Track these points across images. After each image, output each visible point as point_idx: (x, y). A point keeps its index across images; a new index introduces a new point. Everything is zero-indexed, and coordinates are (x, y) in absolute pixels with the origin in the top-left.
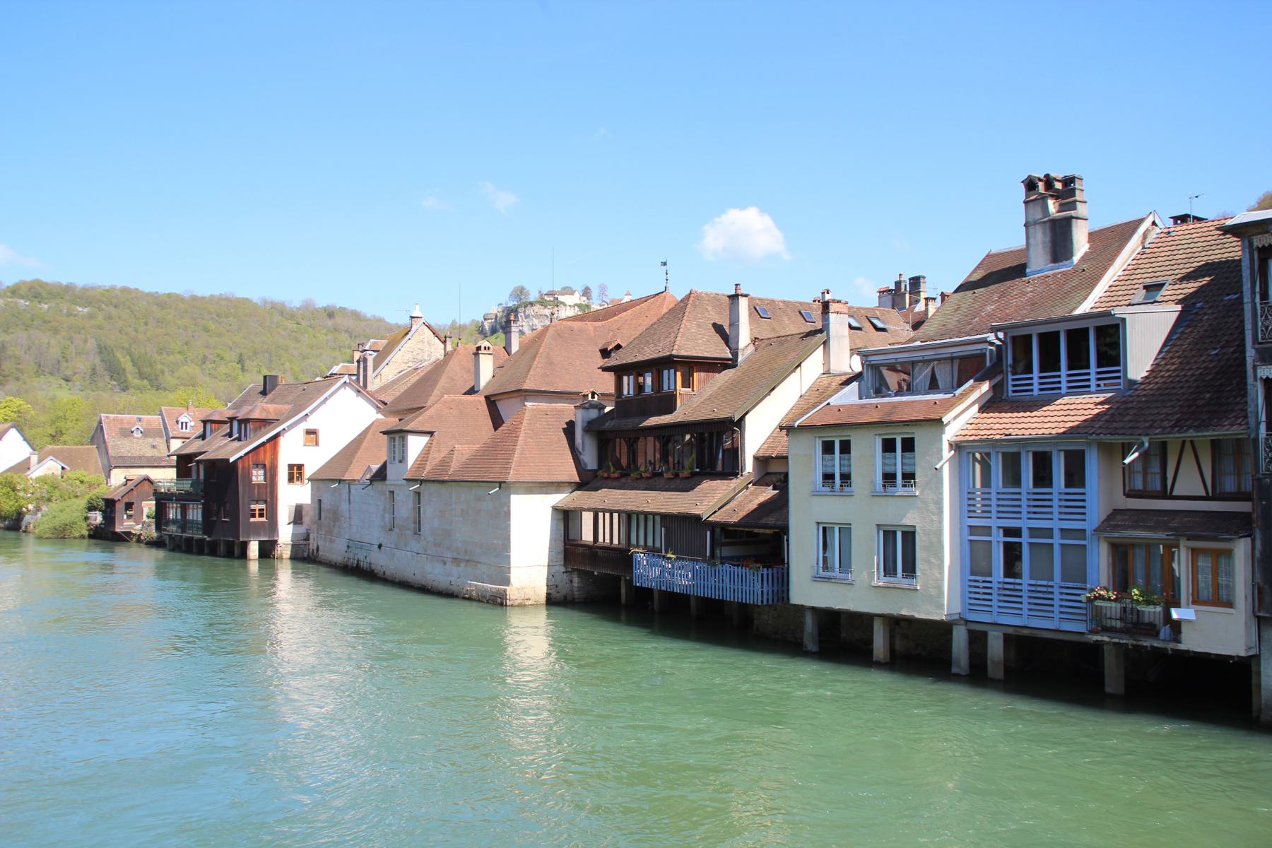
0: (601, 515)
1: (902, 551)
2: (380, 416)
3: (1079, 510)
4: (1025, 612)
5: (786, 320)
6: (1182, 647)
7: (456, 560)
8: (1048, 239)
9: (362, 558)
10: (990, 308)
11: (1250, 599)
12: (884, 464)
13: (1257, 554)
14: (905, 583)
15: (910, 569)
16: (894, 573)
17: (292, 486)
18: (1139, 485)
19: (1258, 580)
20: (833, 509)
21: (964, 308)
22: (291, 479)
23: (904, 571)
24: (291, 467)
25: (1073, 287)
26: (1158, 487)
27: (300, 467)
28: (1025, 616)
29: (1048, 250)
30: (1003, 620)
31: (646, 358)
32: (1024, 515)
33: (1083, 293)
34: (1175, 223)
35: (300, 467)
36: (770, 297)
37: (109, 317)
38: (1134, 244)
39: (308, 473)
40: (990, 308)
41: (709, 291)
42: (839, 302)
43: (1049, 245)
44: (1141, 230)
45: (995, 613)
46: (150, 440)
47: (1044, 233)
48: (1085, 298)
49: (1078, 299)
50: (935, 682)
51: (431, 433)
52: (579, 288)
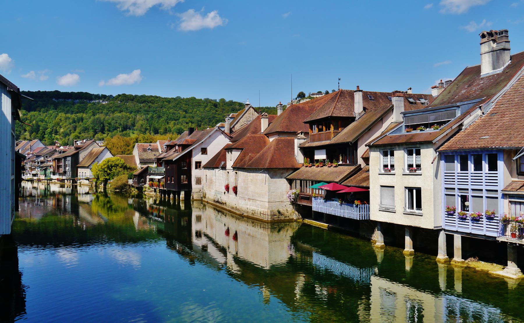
0: (308, 182)
1: (415, 196)
2: (230, 143)
3: (494, 181)
5: (381, 101)
7: (249, 199)
8: (491, 59)
12: (413, 161)
14: (417, 212)
15: (419, 206)
17: (198, 170)
21: (452, 92)
22: (196, 168)
23: (416, 207)
24: (196, 163)
25: (501, 80)
27: (200, 163)
28: (470, 228)
29: (491, 64)
30: (460, 230)
31: (320, 118)
33: (505, 83)
35: (200, 163)
36: (374, 91)
37: (149, 107)
39: (203, 164)
40: (463, 91)
42: (400, 92)
45: (457, 227)
46: (154, 153)
47: (489, 57)
48: (506, 86)
49: (502, 86)
50: (13, 160)
51: (242, 149)
52: (324, 91)
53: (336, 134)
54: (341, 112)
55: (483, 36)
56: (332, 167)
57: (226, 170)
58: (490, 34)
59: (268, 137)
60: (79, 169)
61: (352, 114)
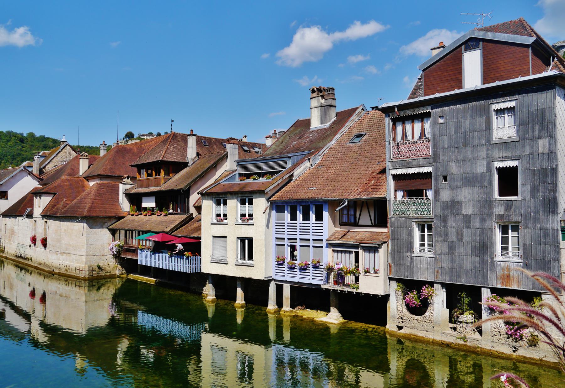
0: (134, 232)
1: (247, 246)
3: (319, 230)
4: (311, 277)
6: (359, 291)
7: (62, 253)
8: (319, 114)
9: (23, 252)
10: (294, 143)
11: (386, 270)
13: (390, 251)
15: (251, 257)
16: (244, 259)
18: (345, 219)
19: (390, 261)
20: (219, 230)
26: (353, 221)
32: (311, 233)
33: (331, 138)
34: (373, 110)
36: (209, 137)
38: (354, 117)
40: (294, 143)
41: (181, 132)
42: (234, 139)
43: (320, 117)
44: (357, 112)
48: (332, 140)
51: (55, 194)
53: (166, 180)
54: (173, 156)
55: (313, 91)
56: (161, 216)
57: (32, 218)
58: (319, 90)
59: (88, 180)
60: (482, 289)
61: (184, 159)
